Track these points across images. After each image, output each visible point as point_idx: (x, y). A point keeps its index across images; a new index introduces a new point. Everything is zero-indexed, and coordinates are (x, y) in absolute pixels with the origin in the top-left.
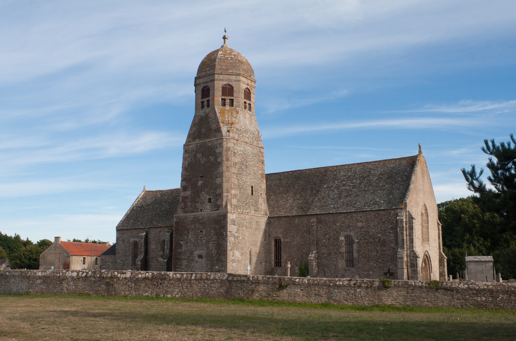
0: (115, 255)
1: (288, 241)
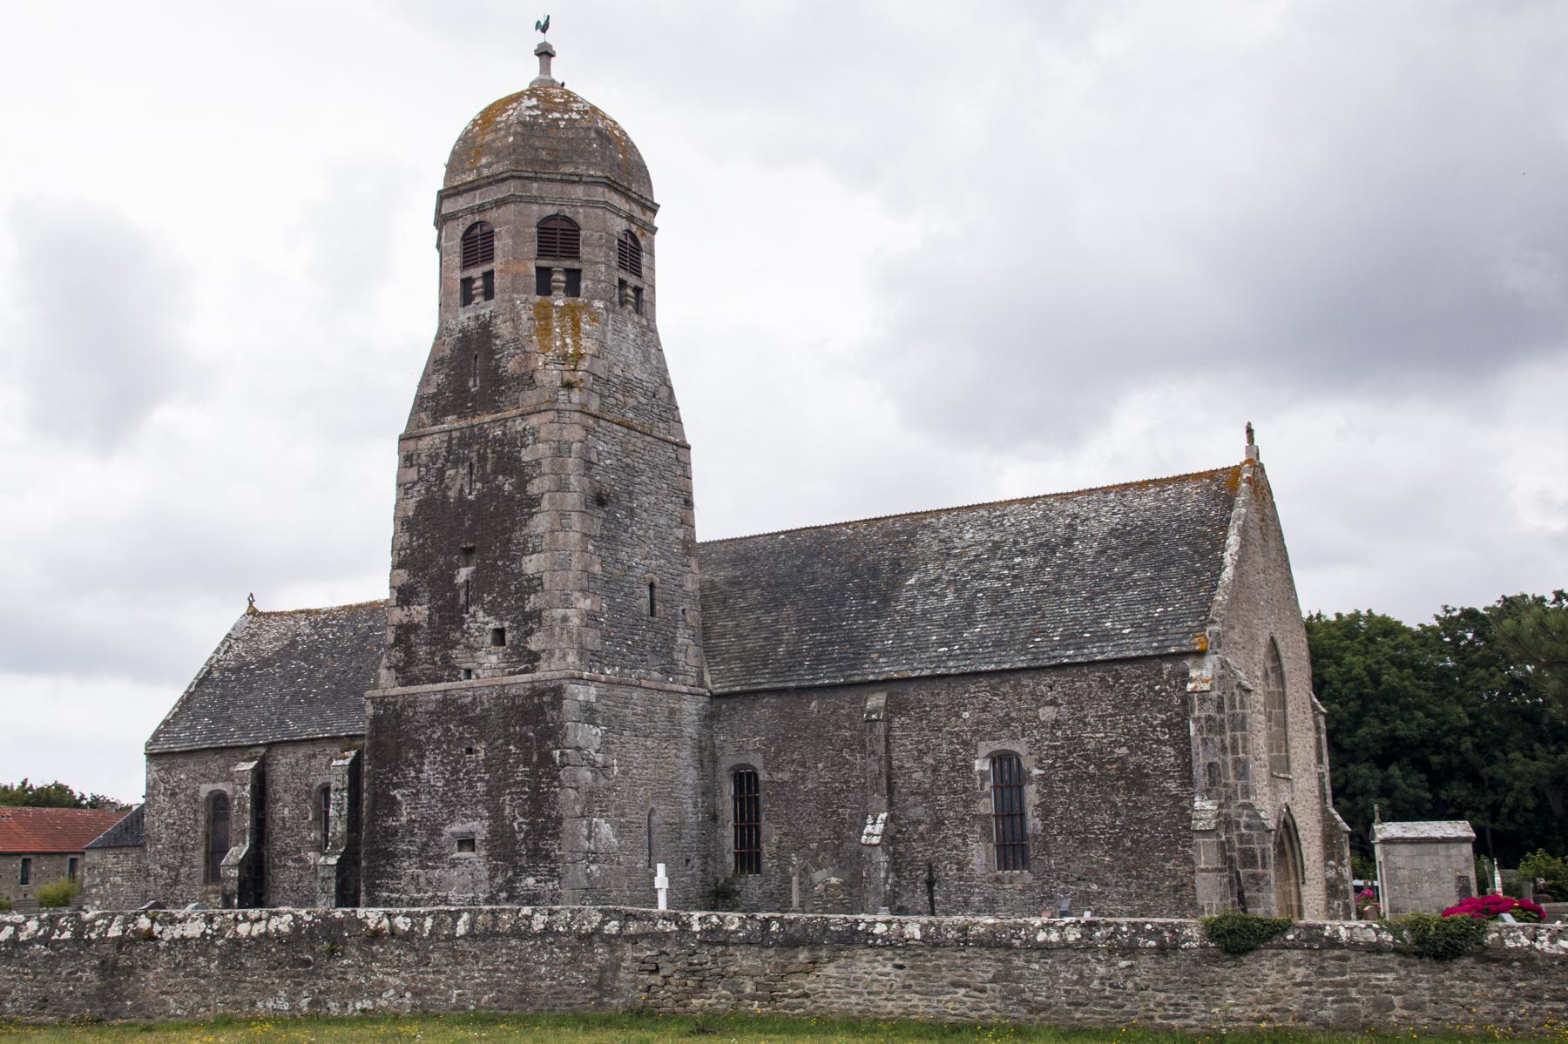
0: (142, 846)
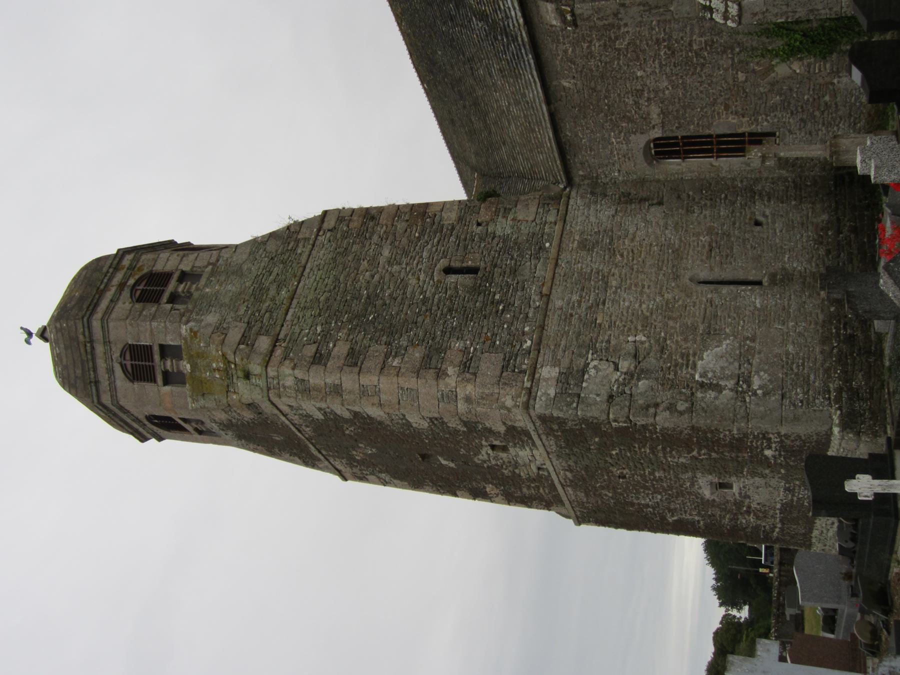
1: (658, 110)
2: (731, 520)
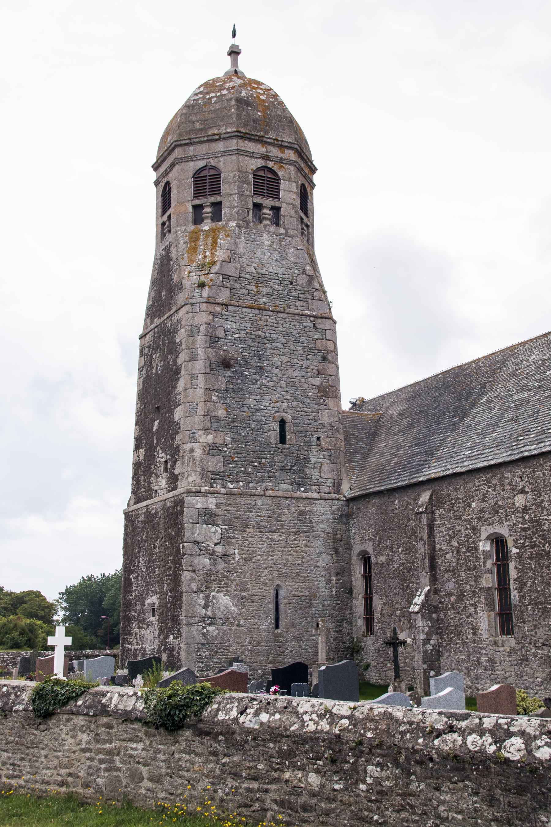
2: (134, 616)
